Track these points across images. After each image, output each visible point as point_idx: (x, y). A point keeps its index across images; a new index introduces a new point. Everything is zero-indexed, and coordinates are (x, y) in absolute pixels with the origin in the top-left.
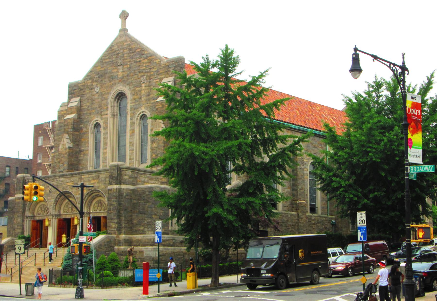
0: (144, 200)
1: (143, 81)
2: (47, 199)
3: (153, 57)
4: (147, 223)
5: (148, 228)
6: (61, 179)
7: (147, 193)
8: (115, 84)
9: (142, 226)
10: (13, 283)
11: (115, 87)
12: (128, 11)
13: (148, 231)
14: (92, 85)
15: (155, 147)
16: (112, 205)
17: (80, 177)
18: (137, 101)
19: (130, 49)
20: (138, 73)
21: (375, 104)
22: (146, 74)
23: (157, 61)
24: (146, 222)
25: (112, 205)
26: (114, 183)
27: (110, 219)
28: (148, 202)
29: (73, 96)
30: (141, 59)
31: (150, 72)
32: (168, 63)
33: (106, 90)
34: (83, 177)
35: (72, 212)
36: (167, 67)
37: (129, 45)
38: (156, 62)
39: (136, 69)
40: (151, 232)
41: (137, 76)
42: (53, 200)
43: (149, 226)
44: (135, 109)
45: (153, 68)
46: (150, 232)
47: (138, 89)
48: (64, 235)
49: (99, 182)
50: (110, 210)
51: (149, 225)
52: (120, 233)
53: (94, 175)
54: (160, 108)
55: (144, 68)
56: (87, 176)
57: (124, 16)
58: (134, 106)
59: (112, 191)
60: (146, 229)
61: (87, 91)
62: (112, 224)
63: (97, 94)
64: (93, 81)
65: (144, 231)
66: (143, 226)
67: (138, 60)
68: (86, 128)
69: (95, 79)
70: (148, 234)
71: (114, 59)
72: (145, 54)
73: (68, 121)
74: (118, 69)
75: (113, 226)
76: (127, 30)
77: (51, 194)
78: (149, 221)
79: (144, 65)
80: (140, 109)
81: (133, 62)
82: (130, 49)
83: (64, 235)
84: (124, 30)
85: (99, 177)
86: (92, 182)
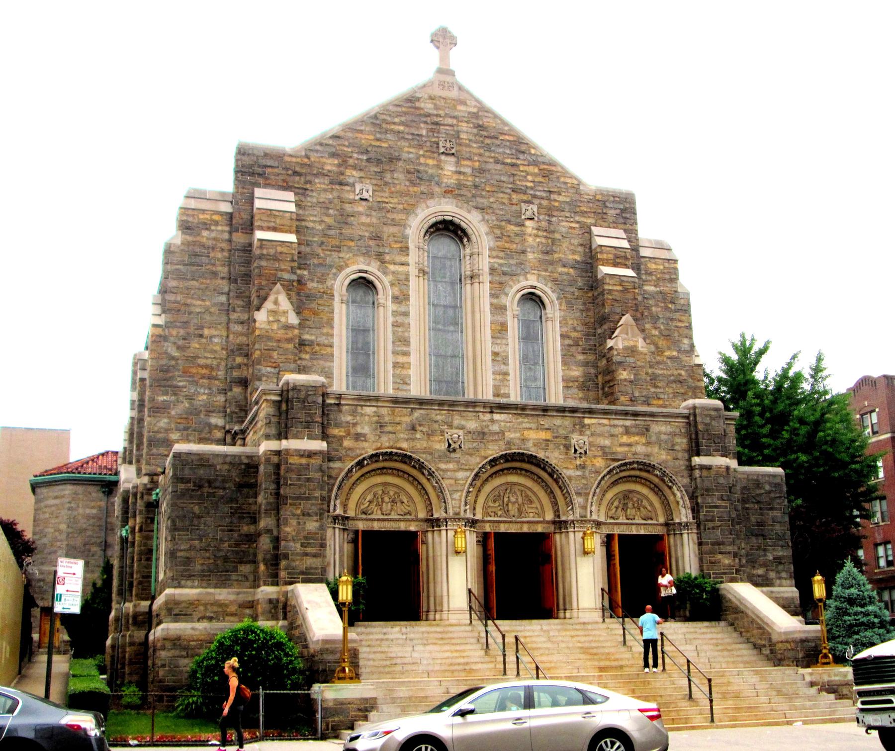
0: (758, 502)
1: (529, 214)
2: (438, 469)
3: (553, 168)
4: (774, 558)
5: (778, 572)
6: (496, 417)
7: (767, 487)
8: (431, 195)
9: (761, 566)
10: (717, 727)
11: (430, 202)
12: (434, 28)
13: (780, 578)
14: (342, 174)
15: (625, 380)
16: (716, 507)
17: (577, 420)
18: (510, 254)
19: (479, 126)
20: (508, 191)
21: (792, 381)
22: (537, 201)
23: (569, 180)
24: (771, 558)
25: (716, 507)
26: (717, 451)
27: (713, 544)
28: (772, 509)
29: (261, 181)
30: (519, 162)
31: (549, 199)
32: (601, 194)
33: (396, 200)
34: (587, 421)
35: (520, 516)
36: (600, 204)
37: (476, 116)
38: (565, 183)
39: (504, 178)
40: (788, 582)
41: (507, 196)
42: (464, 476)
43: (781, 567)
44: (505, 274)
45: (559, 194)
46: (784, 582)
47: (512, 228)
48: (818, 578)
49: (648, 443)
50: (712, 520)
51: (780, 563)
52: (256, 585)
53: (628, 423)
54: (617, 291)
55: (529, 184)
56: (605, 422)
57: (443, 39)
58: (501, 265)
59: (713, 473)
60: (772, 575)
61: (320, 183)
62: (720, 556)
63: (364, 203)
64: (344, 163)
65: (767, 579)
66: (764, 565)
67: (509, 161)
68: (322, 280)
69: (351, 161)
70: (780, 586)
71: (424, 132)
72: (530, 154)
73: (279, 249)
74: (440, 161)
75: (727, 562)
76: (451, 73)
77: (453, 455)
78: (781, 553)
79: (530, 178)
80: (521, 278)
81: (491, 160)
82: (480, 127)
83: (818, 578)
84: (444, 71)
85: (647, 430)
86: (625, 439)
